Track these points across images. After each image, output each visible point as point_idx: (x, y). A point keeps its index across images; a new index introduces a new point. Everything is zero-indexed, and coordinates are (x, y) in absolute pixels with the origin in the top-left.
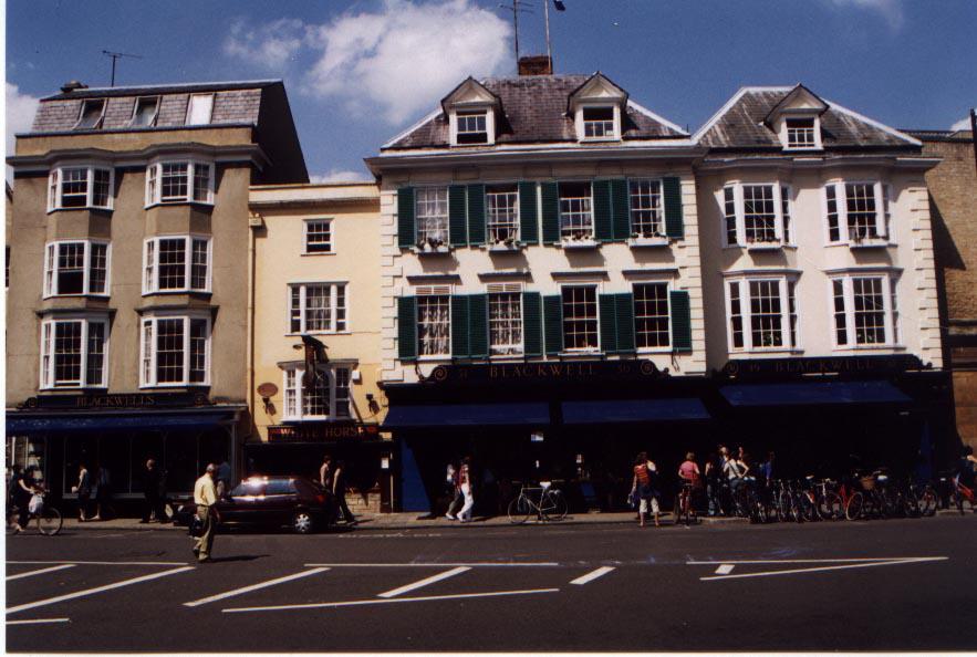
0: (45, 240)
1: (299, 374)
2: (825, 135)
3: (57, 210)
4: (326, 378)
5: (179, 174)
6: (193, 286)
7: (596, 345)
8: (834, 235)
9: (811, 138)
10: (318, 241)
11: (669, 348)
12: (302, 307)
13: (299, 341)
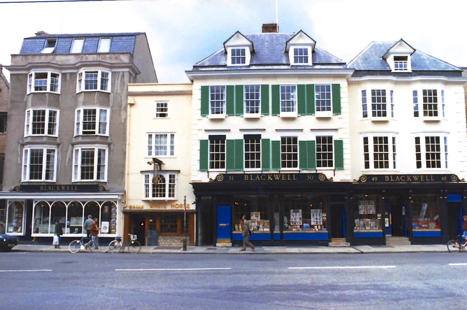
1: (151, 176)
2: (413, 65)
3: (82, 92)
4: (164, 181)
5: (93, 79)
7: (332, 166)
8: (365, 115)
9: (405, 66)
10: (162, 111)
11: (333, 168)
12: (153, 144)
13: (151, 160)
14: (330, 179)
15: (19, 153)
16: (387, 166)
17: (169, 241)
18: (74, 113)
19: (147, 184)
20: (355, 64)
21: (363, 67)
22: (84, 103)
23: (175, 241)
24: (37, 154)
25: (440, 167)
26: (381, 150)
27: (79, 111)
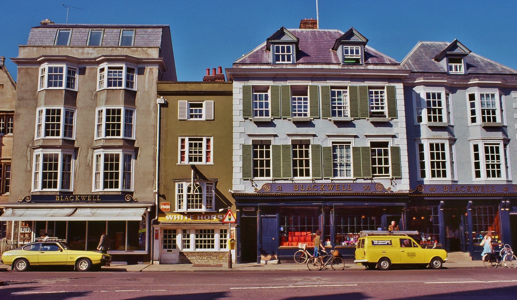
0: (37, 107)
6: (125, 136)
8: (474, 120)
14: (388, 189)
15: (29, 159)
16: (445, 175)
17: (206, 258)
18: (95, 114)
19: (180, 194)
20: (405, 65)
21: (415, 68)
22: (107, 102)
23: (212, 258)
24: (51, 160)
25: (480, 177)
26: (438, 158)
27: (100, 112)
